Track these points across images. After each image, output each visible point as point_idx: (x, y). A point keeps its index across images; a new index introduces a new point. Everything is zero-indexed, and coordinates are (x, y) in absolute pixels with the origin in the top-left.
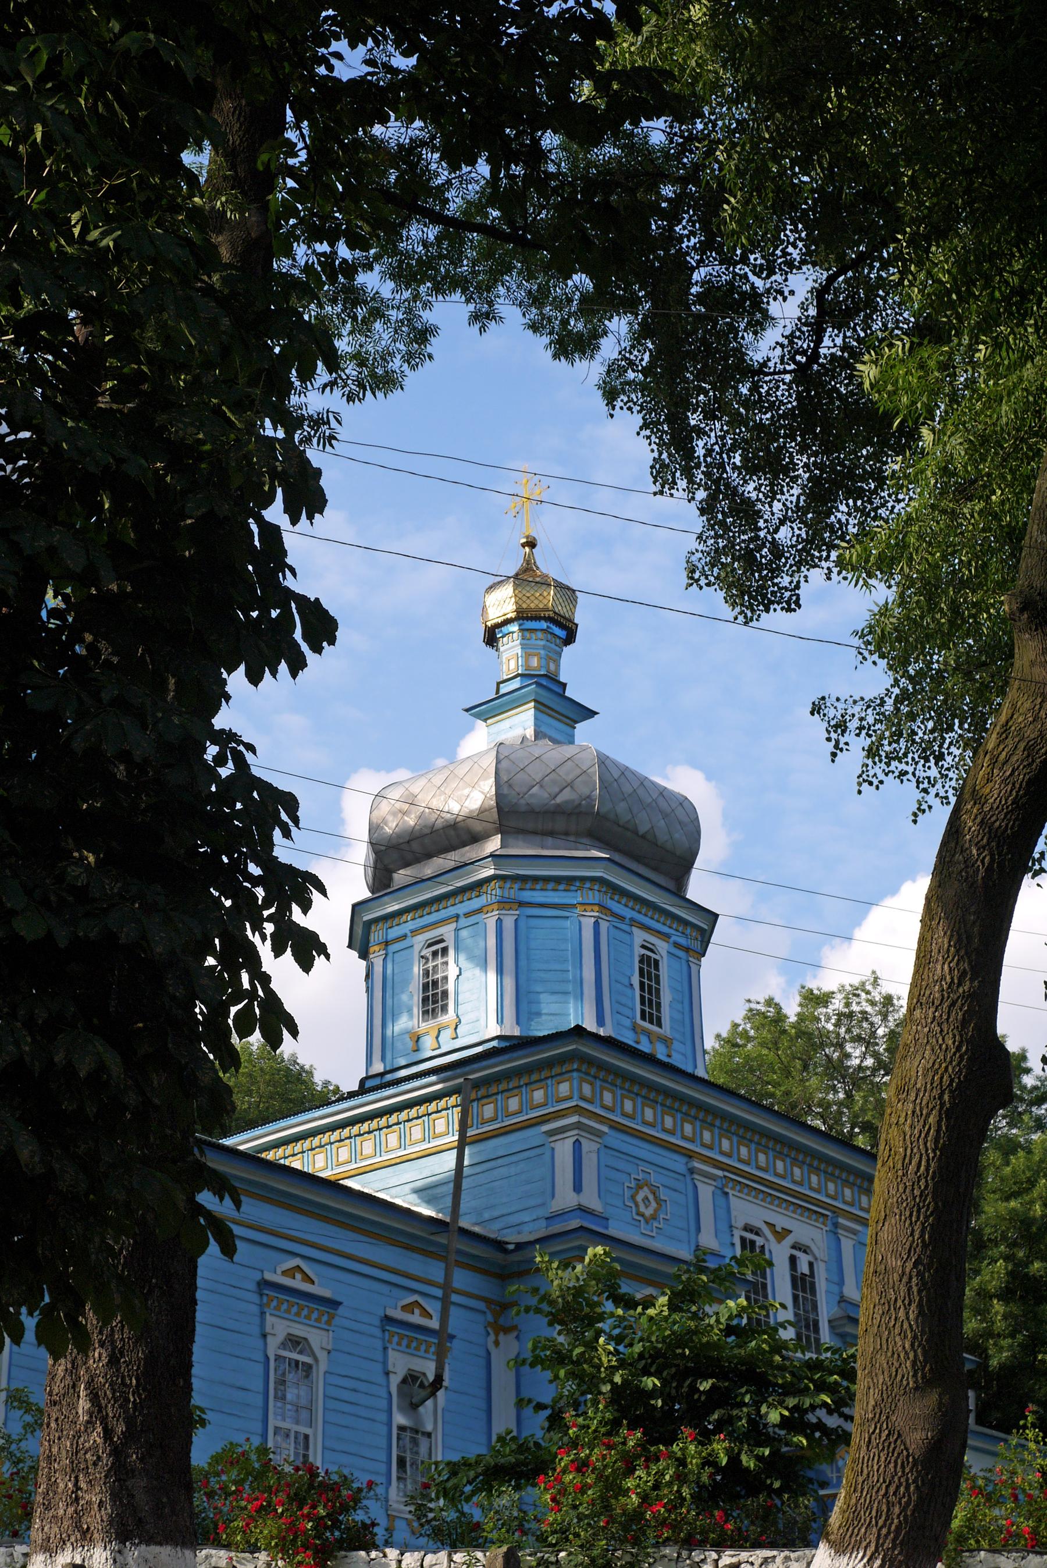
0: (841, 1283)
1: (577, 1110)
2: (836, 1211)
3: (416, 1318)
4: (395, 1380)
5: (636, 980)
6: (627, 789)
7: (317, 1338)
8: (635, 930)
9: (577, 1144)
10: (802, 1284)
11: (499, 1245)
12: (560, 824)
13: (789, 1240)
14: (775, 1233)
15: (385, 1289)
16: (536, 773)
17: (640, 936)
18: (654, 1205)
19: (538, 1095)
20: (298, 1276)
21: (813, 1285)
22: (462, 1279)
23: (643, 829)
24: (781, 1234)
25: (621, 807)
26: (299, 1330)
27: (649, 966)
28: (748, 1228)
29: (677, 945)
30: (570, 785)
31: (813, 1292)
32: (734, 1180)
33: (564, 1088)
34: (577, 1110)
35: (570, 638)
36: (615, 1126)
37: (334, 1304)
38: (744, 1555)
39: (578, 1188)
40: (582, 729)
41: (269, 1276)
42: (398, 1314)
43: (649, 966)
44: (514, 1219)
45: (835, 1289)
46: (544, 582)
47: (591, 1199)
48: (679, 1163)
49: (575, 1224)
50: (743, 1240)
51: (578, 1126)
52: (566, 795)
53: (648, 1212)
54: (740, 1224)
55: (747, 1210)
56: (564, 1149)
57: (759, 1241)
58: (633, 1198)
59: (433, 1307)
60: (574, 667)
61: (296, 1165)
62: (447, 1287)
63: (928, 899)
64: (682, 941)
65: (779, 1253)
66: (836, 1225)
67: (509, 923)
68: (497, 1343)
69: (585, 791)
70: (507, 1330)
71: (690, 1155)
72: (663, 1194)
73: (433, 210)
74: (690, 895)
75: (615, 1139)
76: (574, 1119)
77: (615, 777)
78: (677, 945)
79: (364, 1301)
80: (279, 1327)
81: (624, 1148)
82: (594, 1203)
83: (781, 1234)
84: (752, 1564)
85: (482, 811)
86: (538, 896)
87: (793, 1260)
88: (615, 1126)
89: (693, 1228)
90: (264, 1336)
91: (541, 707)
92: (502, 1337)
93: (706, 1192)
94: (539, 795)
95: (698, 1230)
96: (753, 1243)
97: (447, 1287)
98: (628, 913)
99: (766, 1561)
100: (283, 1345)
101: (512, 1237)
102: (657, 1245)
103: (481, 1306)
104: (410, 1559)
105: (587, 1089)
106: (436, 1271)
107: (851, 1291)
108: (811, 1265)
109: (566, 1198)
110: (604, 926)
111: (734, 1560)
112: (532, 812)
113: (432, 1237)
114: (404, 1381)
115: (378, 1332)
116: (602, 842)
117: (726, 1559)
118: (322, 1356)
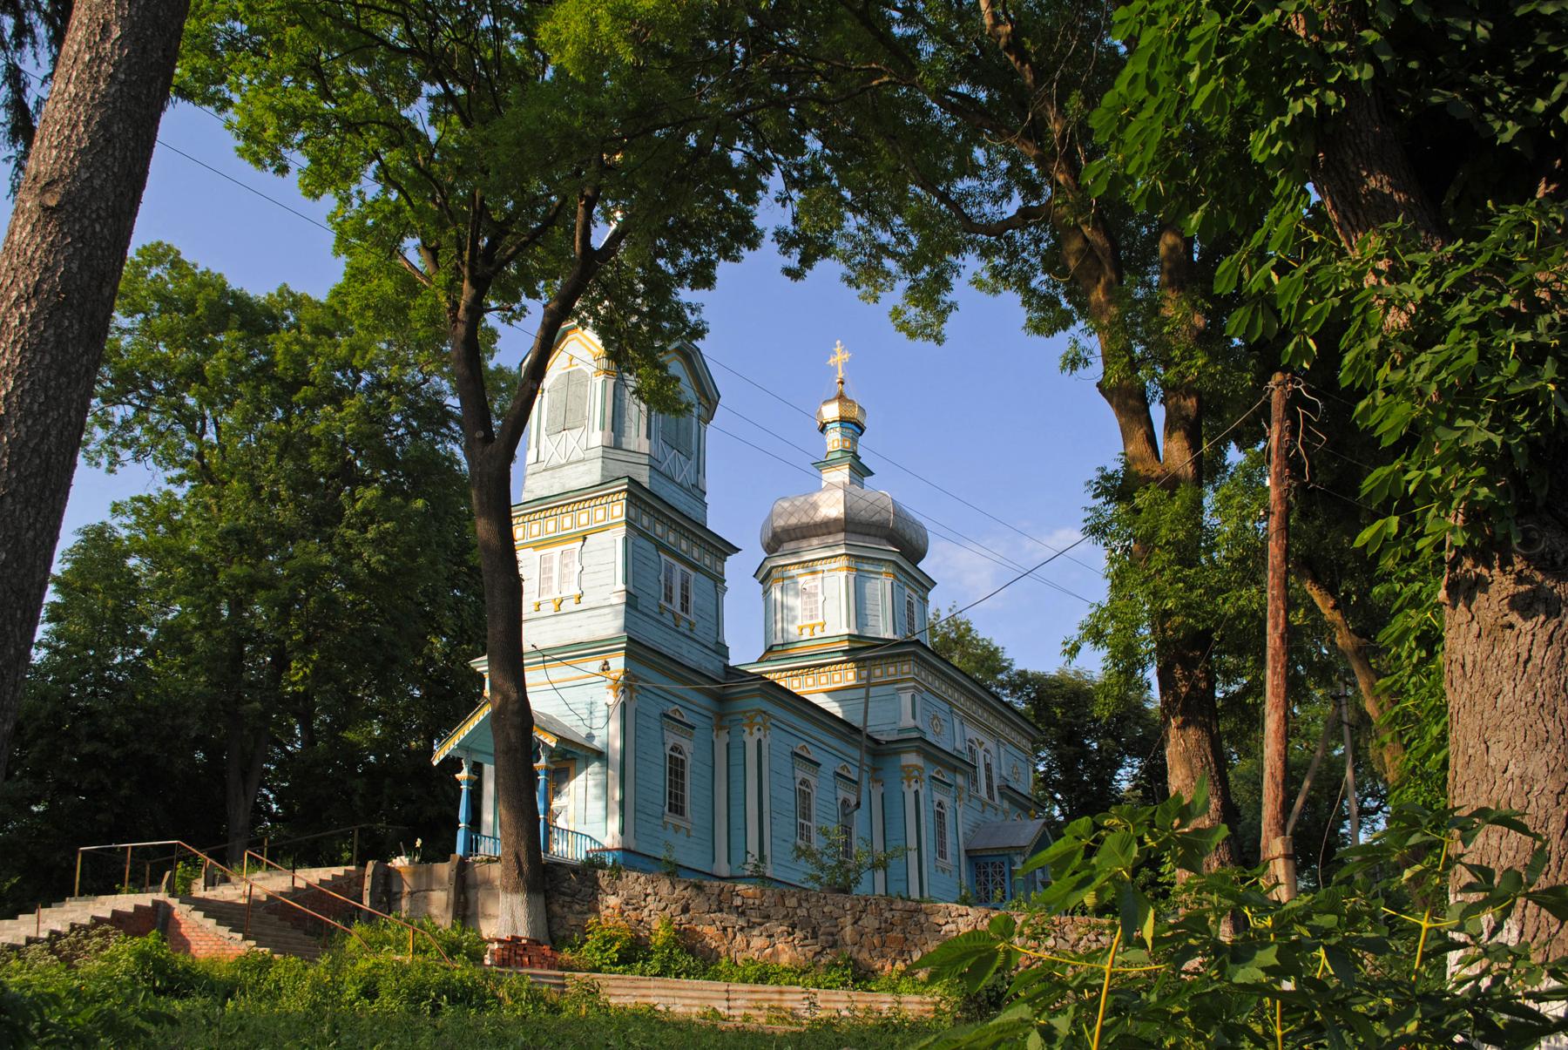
1: (913, 679)
7: (813, 781)
10: (988, 767)
11: (877, 742)
12: (873, 531)
19: (892, 670)
26: (807, 777)
32: (968, 718)
33: (906, 668)
34: (913, 679)
35: (862, 429)
36: (928, 690)
37: (818, 765)
39: (914, 717)
40: (867, 480)
48: (946, 707)
55: (972, 733)
56: (906, 698)
61: (782, 684)
63: (130, 233)
65: (980, 752)
67: (851, 578)
69: (885, 515)
71: (950, 704)
73: (172, 57)
83: (981, 744)
86: (866, 567)
88: (928, 690)
91: (851, 467)
93: (957, 722)
94: (864, 516)
101: (883, 738)
107: (1004, 773)
109: (907, 721)
112: (860, 523)
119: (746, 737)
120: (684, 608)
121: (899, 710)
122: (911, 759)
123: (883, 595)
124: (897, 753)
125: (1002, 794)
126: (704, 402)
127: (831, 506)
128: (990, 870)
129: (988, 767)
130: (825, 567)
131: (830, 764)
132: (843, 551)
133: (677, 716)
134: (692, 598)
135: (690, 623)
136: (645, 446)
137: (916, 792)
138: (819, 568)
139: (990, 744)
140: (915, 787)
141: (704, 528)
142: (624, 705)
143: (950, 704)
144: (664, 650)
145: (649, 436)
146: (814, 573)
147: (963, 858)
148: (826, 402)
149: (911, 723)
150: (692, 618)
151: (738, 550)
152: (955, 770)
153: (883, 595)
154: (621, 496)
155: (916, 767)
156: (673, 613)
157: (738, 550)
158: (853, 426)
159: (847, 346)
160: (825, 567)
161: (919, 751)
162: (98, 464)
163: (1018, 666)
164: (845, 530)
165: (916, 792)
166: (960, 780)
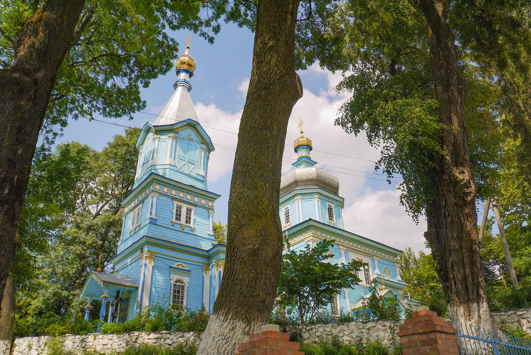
2: (373, 255)
17: (328, 203)
48: (392, 264)
76: (311, 238)
98: (325, 199)
103: (202, 265)
120: (188, 221)
145: (171, 158)
150: (192, 225)
156: (180, 225)
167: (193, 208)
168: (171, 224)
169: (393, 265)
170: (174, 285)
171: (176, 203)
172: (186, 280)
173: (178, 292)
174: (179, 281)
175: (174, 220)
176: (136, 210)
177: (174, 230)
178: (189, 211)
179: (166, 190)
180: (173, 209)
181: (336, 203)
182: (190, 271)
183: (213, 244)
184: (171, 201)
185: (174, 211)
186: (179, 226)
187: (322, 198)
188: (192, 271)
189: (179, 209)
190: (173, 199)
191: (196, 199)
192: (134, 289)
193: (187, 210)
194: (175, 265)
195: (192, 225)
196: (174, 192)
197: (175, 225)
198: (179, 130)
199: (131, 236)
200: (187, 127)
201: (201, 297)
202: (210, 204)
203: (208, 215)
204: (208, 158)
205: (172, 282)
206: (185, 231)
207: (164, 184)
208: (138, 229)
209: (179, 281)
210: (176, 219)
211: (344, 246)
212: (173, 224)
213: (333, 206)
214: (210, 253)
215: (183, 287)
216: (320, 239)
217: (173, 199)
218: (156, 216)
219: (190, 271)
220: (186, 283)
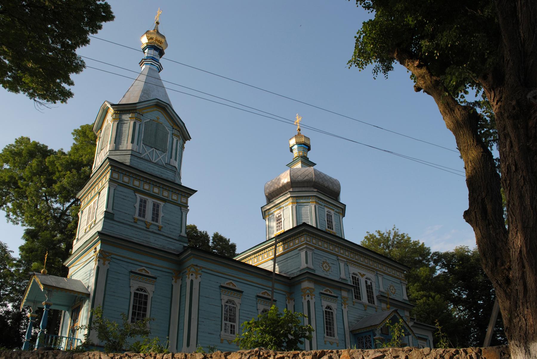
0: (379, 287)
1: (306, 244)
2: (376, 270)
3: (266, 296)
4: (260, 311)
5: (326, 219)
6: (322, 176)
7: (237, 301)
8: (325, 208)
9: (306, 252)
10: (369, 288)
13: (365, 277)
14: (361, 275)
15: (257, 288)
16: (299, 173)
17: (326, 209)
18: (328, 267)
19: (297, 241)
20: (231, 285)
21: (372, 288)
22: (277, 286)
23: (326, 186)
24: (363, 275)
25: (320, 180)
27: (329, 216)
28: (353, 274)
29: (336, 212)
30: (307, 175)
31: (372, 289)
32: (348, 262)
33: (303, 239)
34: (306, 244)
35: (309, 149)
36: (316, 248)
37: (242, 292)
38: (285, 354)
39: (307, 263)
41: (222, 285)
42: (261, 295)
43: (329, 216)
44: (292, 272)
45: (378, 289)
46: (302, 136)
47: (310, 265)
48: (335, 258)
49: (306, 271)
50: (353, 277)
51: (306, 247)
52: (307, 178)
53: (326, 269)
54: (352, 272)
55: (353, 269)
56: (303, 254)
57: (357, 277)
58: (322, 266)
59: (270, 293)
60: (311, 156)
62: (273, 288)
64: (337, 211)
65: (362, 281)
66: (377, 273)
67: (294, 207)
68: (289, 303)
69: (311, 177)
70: (291, 299)
71: (337, 256)
72: (330, 265)
74: (341, 202)
75: (316, 251)
76: (305, 246)
77: (318, 174)
78: (336, 212)
79: (251, 292)
80: (225, 298)
81: (319, 253)
82: (311, 266)
83: (363, 275)
84: (289, 357)
85: (287, 183)
86: (302, 201)
87: (366, 282)
88: (316, 248)
89: (339, 273)
90: (221, 300)
91: (302, 162)
92: (290, 301)
93: (342, 265)
94: (300, 178)
95: (340, 274)
96: (355, 277)
97: (273, 288)
98: (323, 204)
99: (295, 356)
100: (326, 308)
102: (330, 277)
104: (415, 355)
105: (308, 239)
106: (270, 284)
108: (371, 283)
109: (304, 265)
110: (317, 207)
111: (281, 355)
113: (88, 207)
114: (263, 312)
115: (255, 299)
116: (316, 188)
117: (279, 355)
118: (238, 305)
119: (303, 300)
121: (301, 261)
122: (306, 284)
123: (311, 212)
124: (300, 282)
125: (380, 301)
126: (176, 127)
127: (285, 179)
128: (364, 340)
129: (369, 288)
130: (284, 205)
131: (251, 292)
132: (289, 196)
133: (231, 287)
134: (161, 214)
135: (158, 226)
136: (130, 146)
137: (308, 302)
138: (282, 206)
139: (369, 275)
140: (191, 277)
141: (180, 186)
142: (98, 268)
143: (337, 256)
144: (135, 240)
145: (132, 142)
146: (280, 208)
147: (348, 336)
148: (290, 139)
149: (306, 266)
150: (160, 223)
151: (196, 191)
152: (340, 289)
153: (311, 212)
154: (109, 169)
155: (309, 289)
156: (145, 222)
157: (196, 191)
158: (306, 146)
159: (299, 116)
160: (284, 205)
161: (310, 280)
162: (17, 224)
163: (433, 251)
164: (292, 187)
165: (308, 302)
166: (344, 294)
167: (162, 204)
168: (132, 221)
169: (399, 282)
170: (135, 293)
171: (139, 196)
172: (150, 288)
173: (140, 303)
174: (142, 290)
175: (136, 216)
176: (92, 203)
177: (136, 227)
178: (156, 208)
179: (126, 179)
180: (136, 202)
181: (336, 210)
182: (155, 278)
183: (184, 247)
184: (134, 194)
185: (137, 205)
186: (143, 224)
187: (320, 202)
188: (158, 278)
189: (143, 203)
190: (136, 190)
191: (166, 194)
192: (84, 296)
193: (154, 205)
194: (137, 269)
195: (160, 223)
196: (137, 183)
197: (138, 222)
198: (145, 111)
199: (86, 233)
200: (155, 109)
201: (169, 310)
202: (184, 200)
203: (180, 213)
204: (183, 148)
205: (133, 290)
206: (150, 230)
207: (145, 180)
208: (93, 225)
209: (142, 290)
210: (140, 215)
211: (344, 258)
212: (135, 221)
213: (332, 212)
214: (182, 257)
215: (146, 296)
216: (108, 167)
217: (136, 190)
218: (113, 209)
219: (155, 278)
220: (237, 304)
